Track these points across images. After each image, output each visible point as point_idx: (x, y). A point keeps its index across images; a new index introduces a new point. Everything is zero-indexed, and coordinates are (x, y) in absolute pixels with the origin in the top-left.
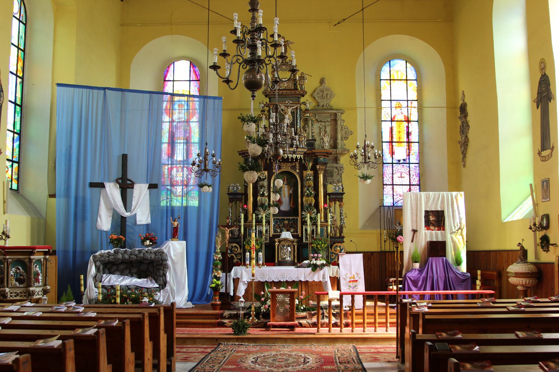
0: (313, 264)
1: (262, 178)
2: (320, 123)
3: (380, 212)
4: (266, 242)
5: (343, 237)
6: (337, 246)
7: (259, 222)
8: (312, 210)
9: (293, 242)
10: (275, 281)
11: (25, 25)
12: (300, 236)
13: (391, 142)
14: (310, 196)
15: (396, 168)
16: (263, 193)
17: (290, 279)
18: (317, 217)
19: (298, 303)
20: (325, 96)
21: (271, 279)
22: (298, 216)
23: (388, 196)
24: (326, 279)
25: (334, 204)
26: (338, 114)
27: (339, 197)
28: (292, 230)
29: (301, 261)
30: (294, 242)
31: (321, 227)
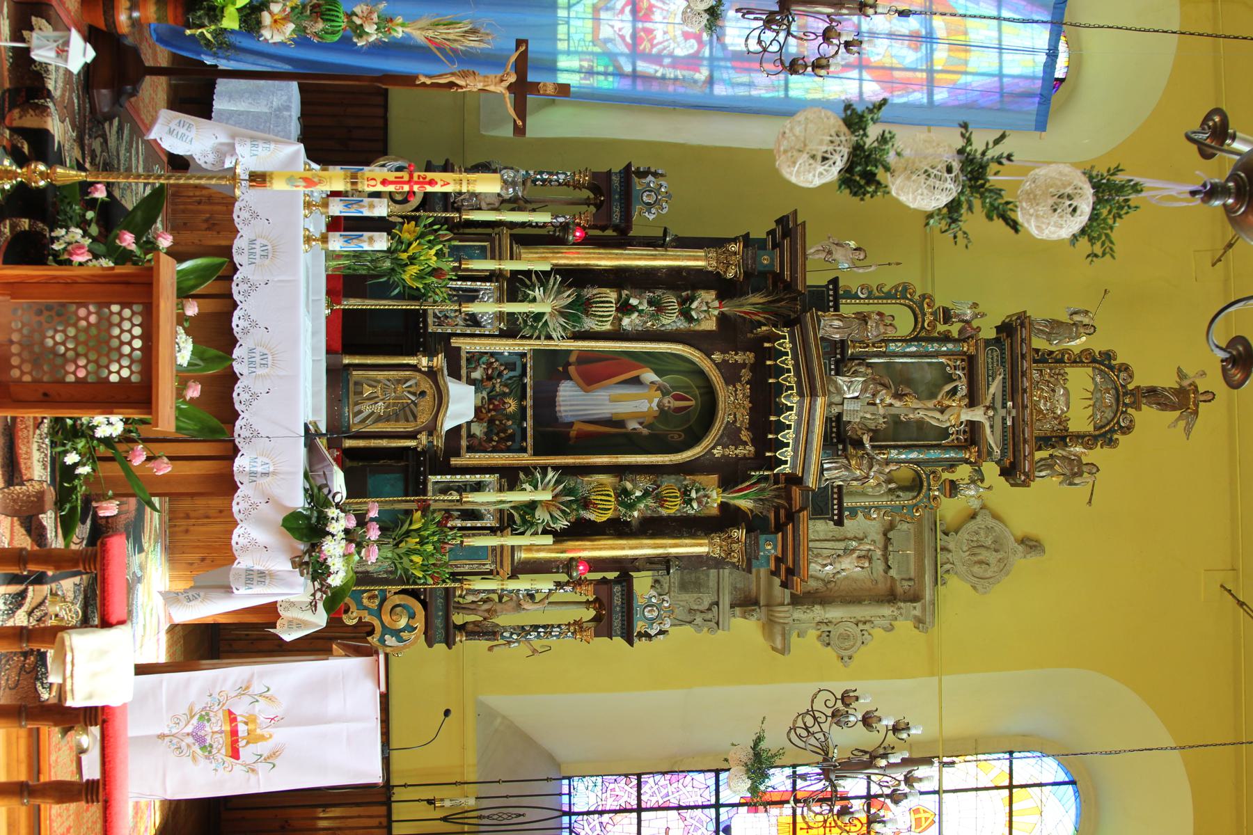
0: (323, 519)
1: (694, 306)
2: (879, 538)
3: (547, 780)
4: (430, 320)
5: (449, 642)
6: (412, 616)
7: (515, 286)
8: (563, 512)
9: (431, 429)
10: (236, 314)
12: (454, 461)
14: (621, 503)
15: (700, 821)
16: (633, 309)
17: (244, 396)
18: (535, 533)
19: (100, 433)
20: (980, 557)
21: (247, 294)
22: (537, 453)
23: (599, 794)
24: (243, 591)
25: (584, 599)
26: (918, 605)
27: (617, 623)
28: (478, 430)
29: (349, 464)
30: (430, 434)
31: (494, 549)
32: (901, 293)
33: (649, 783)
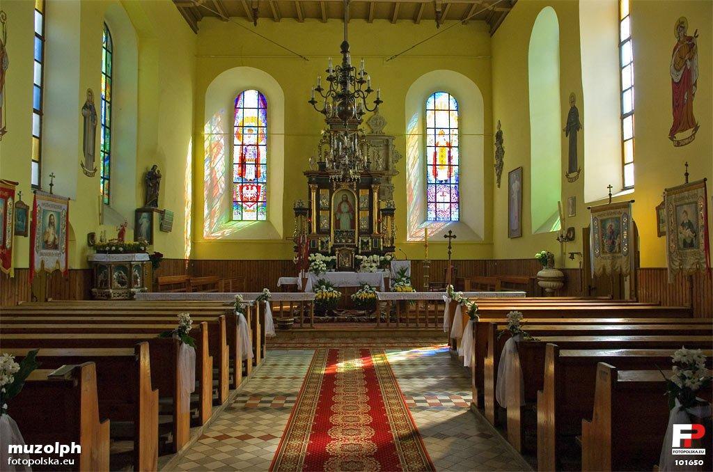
11: (111, 53)
13: (435, 165)
32: (320, 147)
33: (430, 200)
